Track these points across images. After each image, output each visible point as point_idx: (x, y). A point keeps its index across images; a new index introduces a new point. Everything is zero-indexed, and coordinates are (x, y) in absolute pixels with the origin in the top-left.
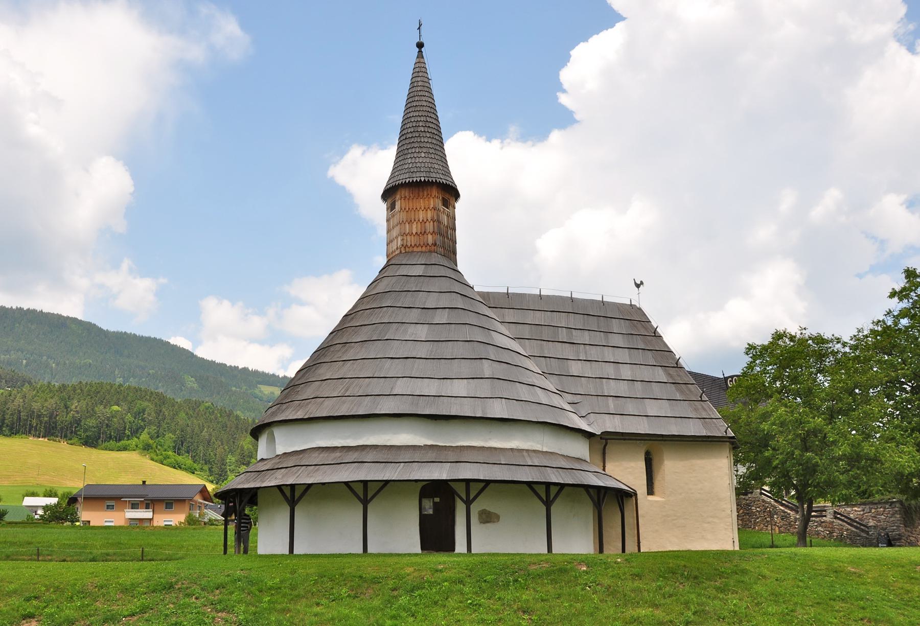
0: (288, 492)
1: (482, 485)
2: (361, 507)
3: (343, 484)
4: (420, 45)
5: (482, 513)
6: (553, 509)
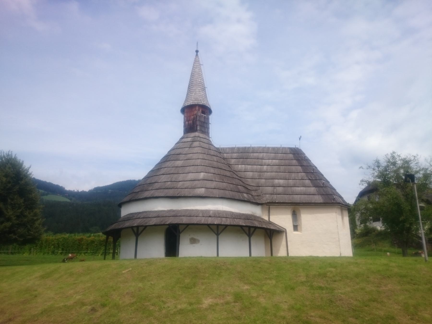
0: (135, 229)
1: (224, 227)
3: (206, 226)
4: (197, 51)
6: (252, 238)
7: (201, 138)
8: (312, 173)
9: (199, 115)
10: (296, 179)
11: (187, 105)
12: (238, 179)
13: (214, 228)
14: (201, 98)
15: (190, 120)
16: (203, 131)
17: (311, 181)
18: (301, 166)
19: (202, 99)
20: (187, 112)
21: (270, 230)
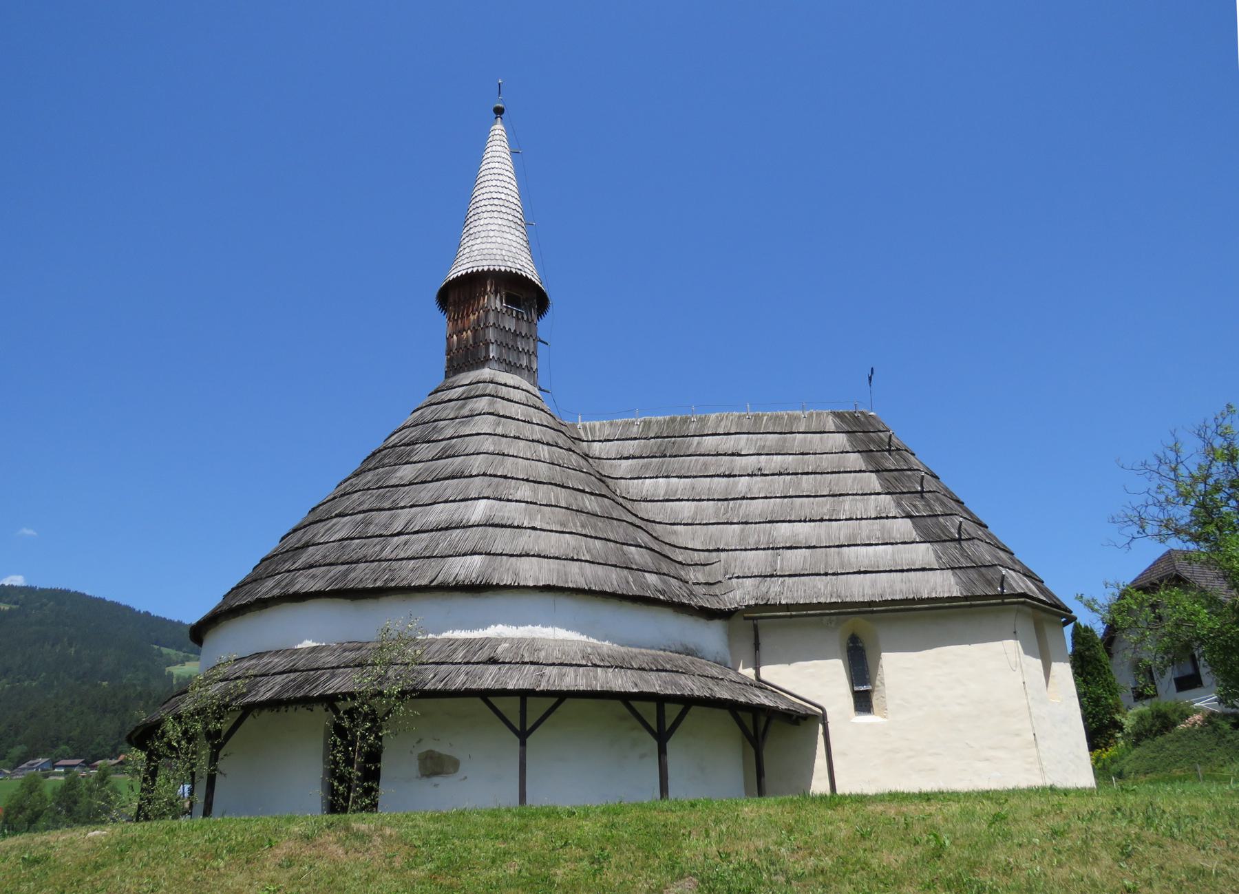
2: (654, 744)
5: (426, 758)
6: (671, 746)
7: (500, 384)
8: (917, 492)
9: (496, 308)
10: (857, 519)
11: (455, 276)
12: (631, 524)
13: (510, 707)
14: (504, 252)
15: (464, 330)
16: (510, 362)
17: (913, 523)
18: (877, 471)
19: (510, 254)
20: (455, 301)
21: (758, 710)
